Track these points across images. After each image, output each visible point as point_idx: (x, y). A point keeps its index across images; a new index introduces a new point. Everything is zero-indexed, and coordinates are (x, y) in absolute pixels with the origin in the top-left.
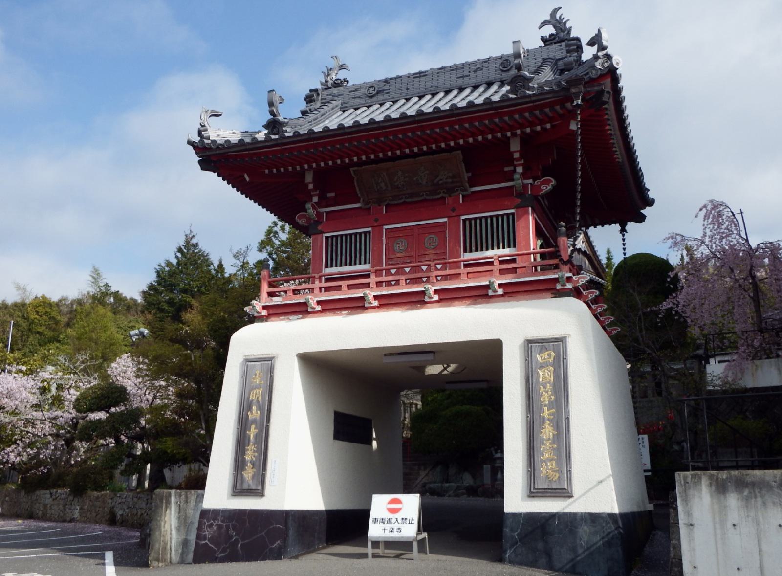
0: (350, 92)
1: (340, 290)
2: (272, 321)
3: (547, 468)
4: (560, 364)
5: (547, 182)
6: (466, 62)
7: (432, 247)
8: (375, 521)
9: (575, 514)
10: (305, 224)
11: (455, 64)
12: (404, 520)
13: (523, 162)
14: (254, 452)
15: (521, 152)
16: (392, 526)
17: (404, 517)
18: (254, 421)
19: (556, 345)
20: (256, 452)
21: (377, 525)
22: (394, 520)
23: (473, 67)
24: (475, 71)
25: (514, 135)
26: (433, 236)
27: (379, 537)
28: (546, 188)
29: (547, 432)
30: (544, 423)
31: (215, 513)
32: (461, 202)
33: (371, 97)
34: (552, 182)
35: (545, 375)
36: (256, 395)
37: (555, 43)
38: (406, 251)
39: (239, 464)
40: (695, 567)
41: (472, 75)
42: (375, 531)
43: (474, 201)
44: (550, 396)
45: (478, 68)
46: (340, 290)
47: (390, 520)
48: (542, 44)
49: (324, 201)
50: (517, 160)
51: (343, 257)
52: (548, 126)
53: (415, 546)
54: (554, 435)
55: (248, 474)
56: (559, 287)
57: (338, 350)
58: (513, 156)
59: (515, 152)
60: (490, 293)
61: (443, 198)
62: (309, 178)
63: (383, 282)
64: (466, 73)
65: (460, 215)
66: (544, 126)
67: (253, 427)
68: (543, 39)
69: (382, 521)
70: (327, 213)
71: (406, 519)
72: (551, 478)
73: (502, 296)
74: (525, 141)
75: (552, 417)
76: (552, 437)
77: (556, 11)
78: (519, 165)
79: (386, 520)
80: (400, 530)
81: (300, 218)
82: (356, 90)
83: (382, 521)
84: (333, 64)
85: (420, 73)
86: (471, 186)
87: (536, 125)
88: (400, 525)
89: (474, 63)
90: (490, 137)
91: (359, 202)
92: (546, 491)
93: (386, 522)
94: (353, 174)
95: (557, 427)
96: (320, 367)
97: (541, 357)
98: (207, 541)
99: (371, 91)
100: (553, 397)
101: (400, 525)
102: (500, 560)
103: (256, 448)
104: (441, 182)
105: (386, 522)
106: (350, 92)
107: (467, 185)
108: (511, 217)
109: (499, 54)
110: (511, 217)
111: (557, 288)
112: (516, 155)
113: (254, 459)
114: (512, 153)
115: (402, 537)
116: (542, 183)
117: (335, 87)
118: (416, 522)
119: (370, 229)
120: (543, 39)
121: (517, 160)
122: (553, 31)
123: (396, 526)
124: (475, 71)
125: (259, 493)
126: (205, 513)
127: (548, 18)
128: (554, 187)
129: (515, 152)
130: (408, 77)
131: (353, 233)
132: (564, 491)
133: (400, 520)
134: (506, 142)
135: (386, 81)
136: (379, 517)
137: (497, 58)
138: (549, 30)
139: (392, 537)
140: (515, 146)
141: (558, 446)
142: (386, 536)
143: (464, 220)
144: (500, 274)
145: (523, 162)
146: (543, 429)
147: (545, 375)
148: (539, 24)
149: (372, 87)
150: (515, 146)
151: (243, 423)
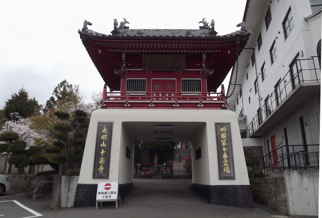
0: (131, 31)
1: (198, 99)
2: (109, 108)
3: (227, 170)
4: (229, 133)
5: (212, 71)
6: (84, 24)
7: (170, 88)
8: (99, 193)
9: (236, 186)
10: (118, 74)
11: (170, 29)
12: (112, 192)
13: (125, 62)
14: (103, 160)
15: (126, 58)
16: (107, 195)
17: (112, 191)
18: (103, 148)
19: (228, 125)
20: (104, 160)
21: (100, 195)
22: (107, 193)
23: (177, 31)
24: (178, 33)
25: (124, 52)
26: (170, 84)
27: (101, 200)
28: (211, 73)
29: (225, 156)
30: (224, 153)
31: (85, 186)
32: (152, 73)
33: (139, 34)
34: (213, 71)
35: (223, 136)
36: (104, 137)
37: (205, 29)
38: (160, 88)
39: (96, 165)
40: (293, 204)
41: (176, 33)
42: (99, 197)
43: (186, 74)
44: (225, 143)
45: (178, 32)
46: (198, 99)
47: (106, 193)
48: (199, 28)
49: (127, 67)
50: (124, 61)
51: (144, 88)
52: (220, 51)
53: (117, 202)
54: (227, 157)
55: (101, 169)
56: (223, 106)
57: (178, 122)
58: (203, 60)
59: (204, 58)
60: (199, 105)
61: (175, 71)
62: (124, 56)
63: (181, 98)
64: (174, 33)
65: (151, 78)
66: (117, 51)
67: (103, 150)
68: (200, 27)
69: (102, 193)
70: (128, 71)
71: (113, 192)
72: (227, 173)
73: (154, 107)
74: (127, 55)
75: (226, 151)
76: (227, 158)
77: (204, 19)
78: (204, 64)
79: (104, 192)
80: (110, 197)
81: (116, 71)
82: (133, 31)
83: (102, 193)
84: (123, 21)
85: (157, 29)
86: (186, 69)
87: (125, 50)
88: (110, 195)
89: (177, 30)
90: (112, 50)
91: (142, 69)
92: (226, 177)
93: (104, 194)
94: (143, 57)
95: (228, 154)
96: (129, 129)
97: (221, 129)
98: (80, 198)
99: (139, 32)
100: (226, 144)
101: (110, 195)
102: (210, 202)
103: (104, 159)
104: (174, 65)
105: (104, 194)
106: (131, 31)
107: (184, 68)
108: (199, 81)
109: (186, 29)
110: (199, 81)
111: (198, 106)
112: (124, 59)
113: (103, 163)
114: (122, 59)
115: (111, 200)
116: (210, 71)
117: (124, 28)
118: (117, 193)
119: (146, 79)
120: (200, 27)
121: (124, 61)
122: (203, 25)
123: (108, 195)
124: (178, 33)
125: (233, 178)
126: (79, 186)
127: (202, 21)
128: (213, 73)
129: (204, 58)
130: (153, 30)
131: (135, 80)
132: (232, 177)
133: (110, 193)
134: (120, 54)
135: (144, 30)
136: (101, 191)
137: (185, 30)
138: (202, 25)
139: (107, 200)
140: (204, 56)
141: (229, 161)
142: (104, 199)
143: (127, 80)
144: (129, 99)
145: (125, 62)
146: (223, 155)
147: (223, 136)
148: (124, 18)
149: (140, 31)
150: (204, 56)
151: (98, 149)
